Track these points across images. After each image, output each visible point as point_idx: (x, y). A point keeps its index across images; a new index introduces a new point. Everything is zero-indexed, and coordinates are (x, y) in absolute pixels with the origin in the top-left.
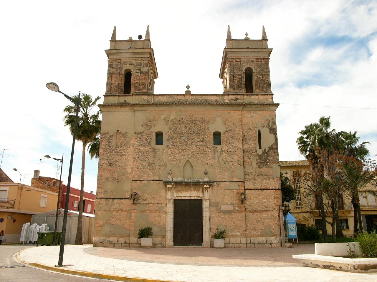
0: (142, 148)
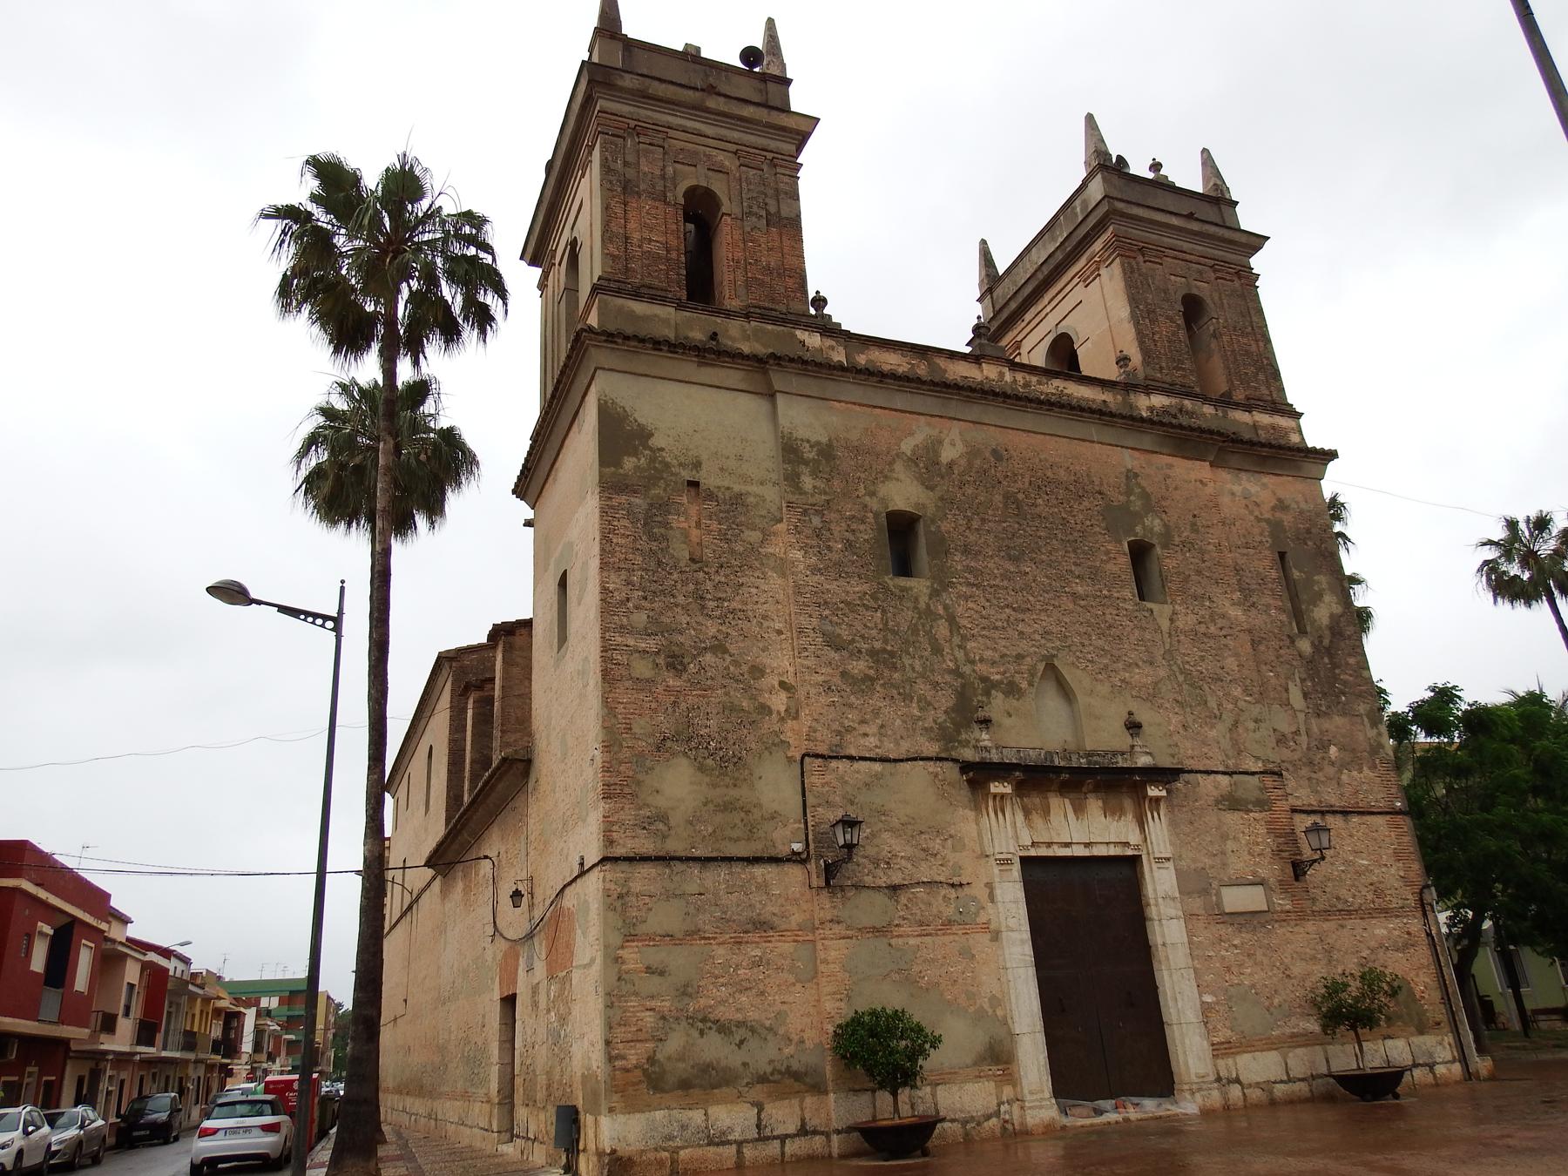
0: (833, 586)
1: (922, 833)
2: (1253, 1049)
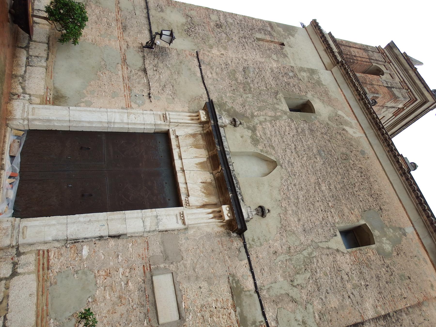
1: (173, 86)
2: (40, 293)
